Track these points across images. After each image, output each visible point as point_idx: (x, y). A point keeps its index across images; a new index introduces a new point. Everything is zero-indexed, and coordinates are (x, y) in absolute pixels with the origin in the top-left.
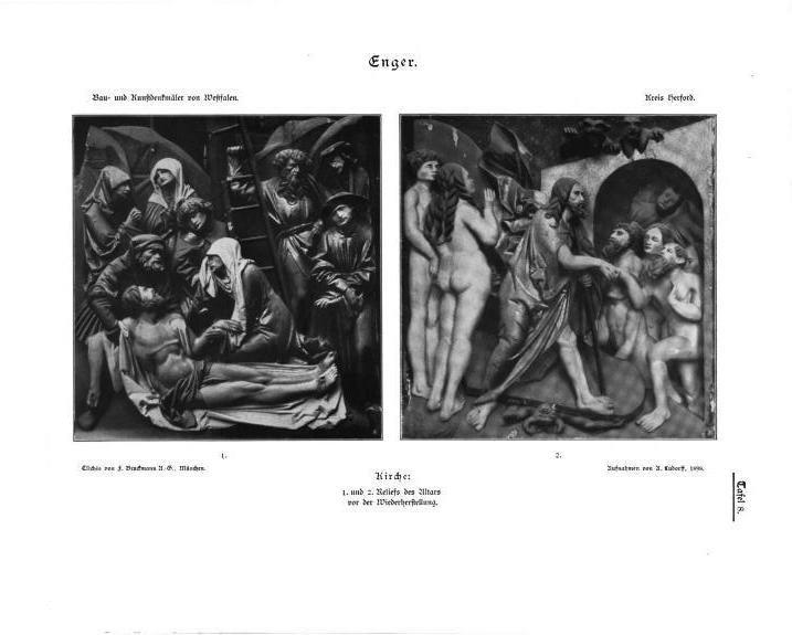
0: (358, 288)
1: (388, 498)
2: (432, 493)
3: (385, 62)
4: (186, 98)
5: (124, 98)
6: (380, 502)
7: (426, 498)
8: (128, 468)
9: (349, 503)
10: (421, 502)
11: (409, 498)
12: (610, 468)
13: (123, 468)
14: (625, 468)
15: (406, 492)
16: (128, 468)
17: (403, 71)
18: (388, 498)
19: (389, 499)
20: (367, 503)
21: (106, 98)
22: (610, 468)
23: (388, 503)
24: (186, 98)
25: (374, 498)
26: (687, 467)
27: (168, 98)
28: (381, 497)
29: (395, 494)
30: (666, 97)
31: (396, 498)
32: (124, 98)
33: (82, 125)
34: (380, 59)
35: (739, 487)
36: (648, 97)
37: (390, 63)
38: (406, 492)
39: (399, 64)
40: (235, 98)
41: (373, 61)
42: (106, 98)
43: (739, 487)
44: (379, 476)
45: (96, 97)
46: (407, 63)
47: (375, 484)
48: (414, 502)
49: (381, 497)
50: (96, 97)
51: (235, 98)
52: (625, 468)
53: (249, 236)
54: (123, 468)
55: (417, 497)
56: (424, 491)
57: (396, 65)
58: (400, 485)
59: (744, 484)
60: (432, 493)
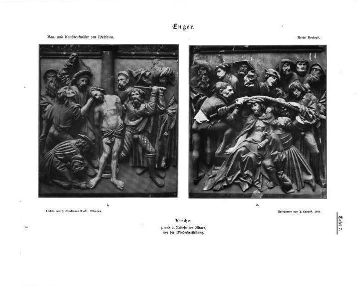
0: (42, 100)
1: (182, 230)
2: (201, 228)
3: (180, 27)
4: (90, 37)
5: (62, 37)
6: (178, 232)
7: (199, 230)
8: (67, 211)
9: (164, 233)
10: (196, 232)
11: (191, 230)
12: (279, 212)
13: (65, 211)
14: (286, 212)
15: (190, 228)
16: (67, 211)
17: (188, 31)
18: (182, 230)
19: (181, 231)
20: (172, 233)
21: (53, 37)
22: (279, 212)
23: (182, 233)
24: (90, 37)
25: (175, 231)
26: (313, 211)
27: (82, 37)
28: (179, 230)
29: (183, 228)
30: (307, 37)
31: (185, 230)
32: (62, 37)
33: (47, 52)
34: (177, 25)
35: (339, 219)
36: (299, 37)
37: (182, 27)
38: (190, 228)
39: (186, 27)
40: (112, 37)
41: (174, 26)
42: (53, 37)
43: (339, 219)
44: (177, 221)
45: (49, 37)
46: (190, 27)
47: (176, 224)
48: (193, 232)
49: (179, 230)
50: (49, 37)
51: (112, 37)
52: (286, 212)
53: (247, 165)
54: (65, 211)
55: (194, 230)
56: (197, 228)
57: (184, 28)
58: (187, 225)
59: (342, 217)
60: (201, 228)
